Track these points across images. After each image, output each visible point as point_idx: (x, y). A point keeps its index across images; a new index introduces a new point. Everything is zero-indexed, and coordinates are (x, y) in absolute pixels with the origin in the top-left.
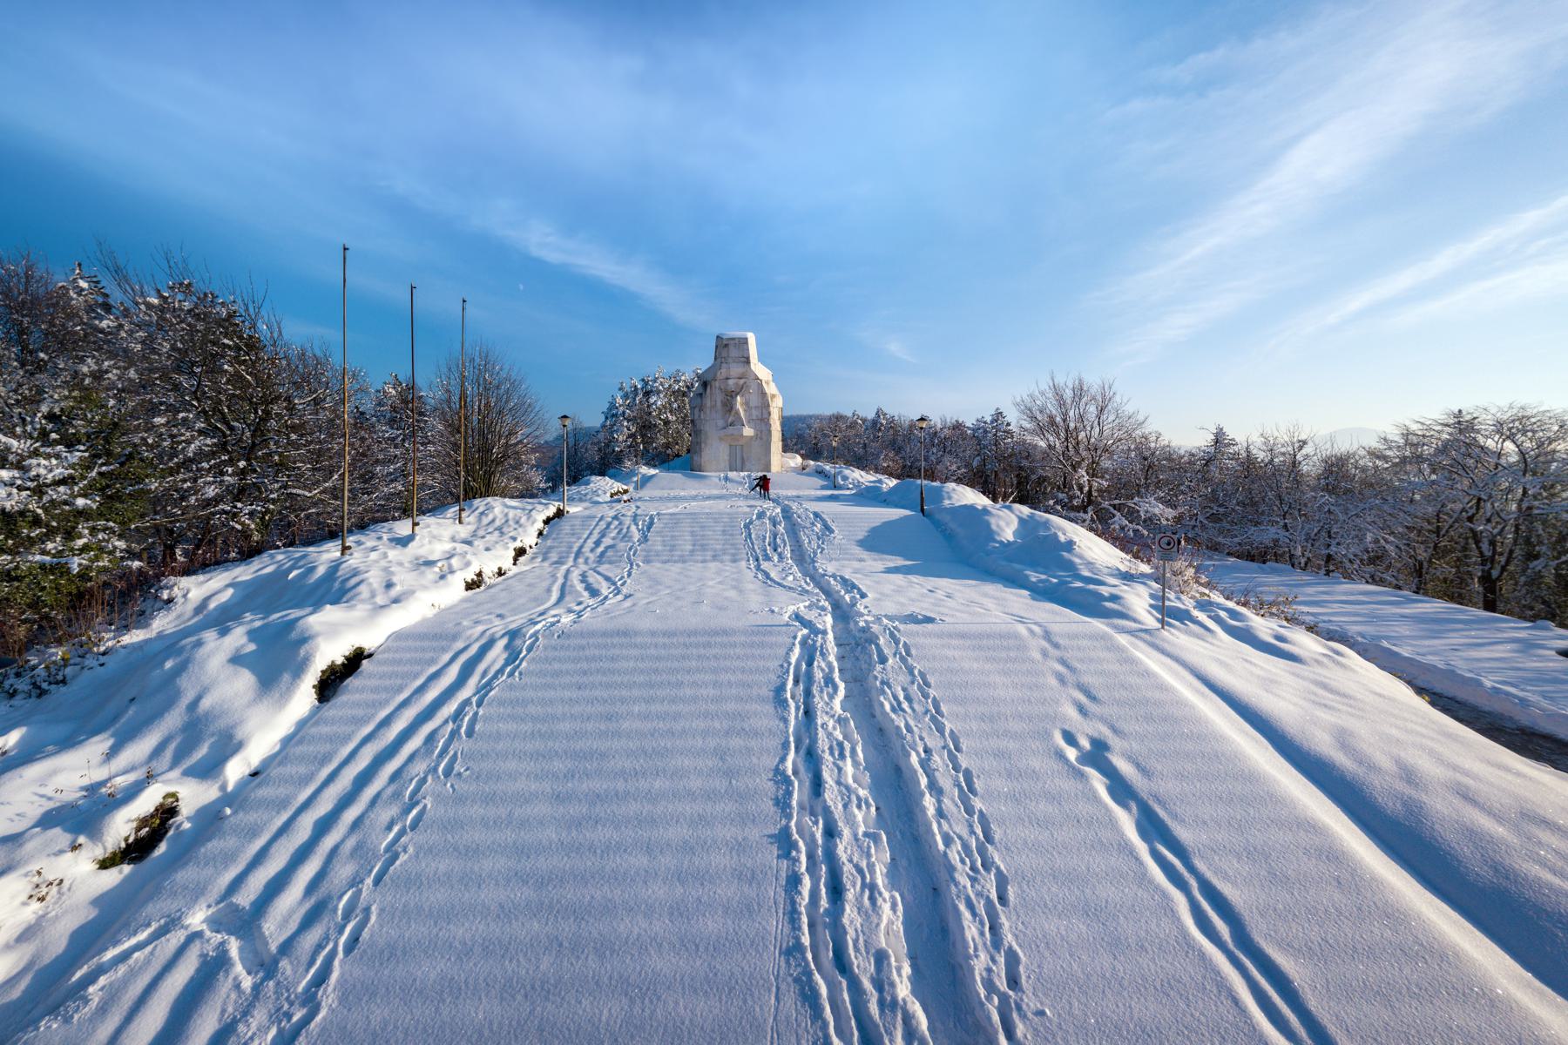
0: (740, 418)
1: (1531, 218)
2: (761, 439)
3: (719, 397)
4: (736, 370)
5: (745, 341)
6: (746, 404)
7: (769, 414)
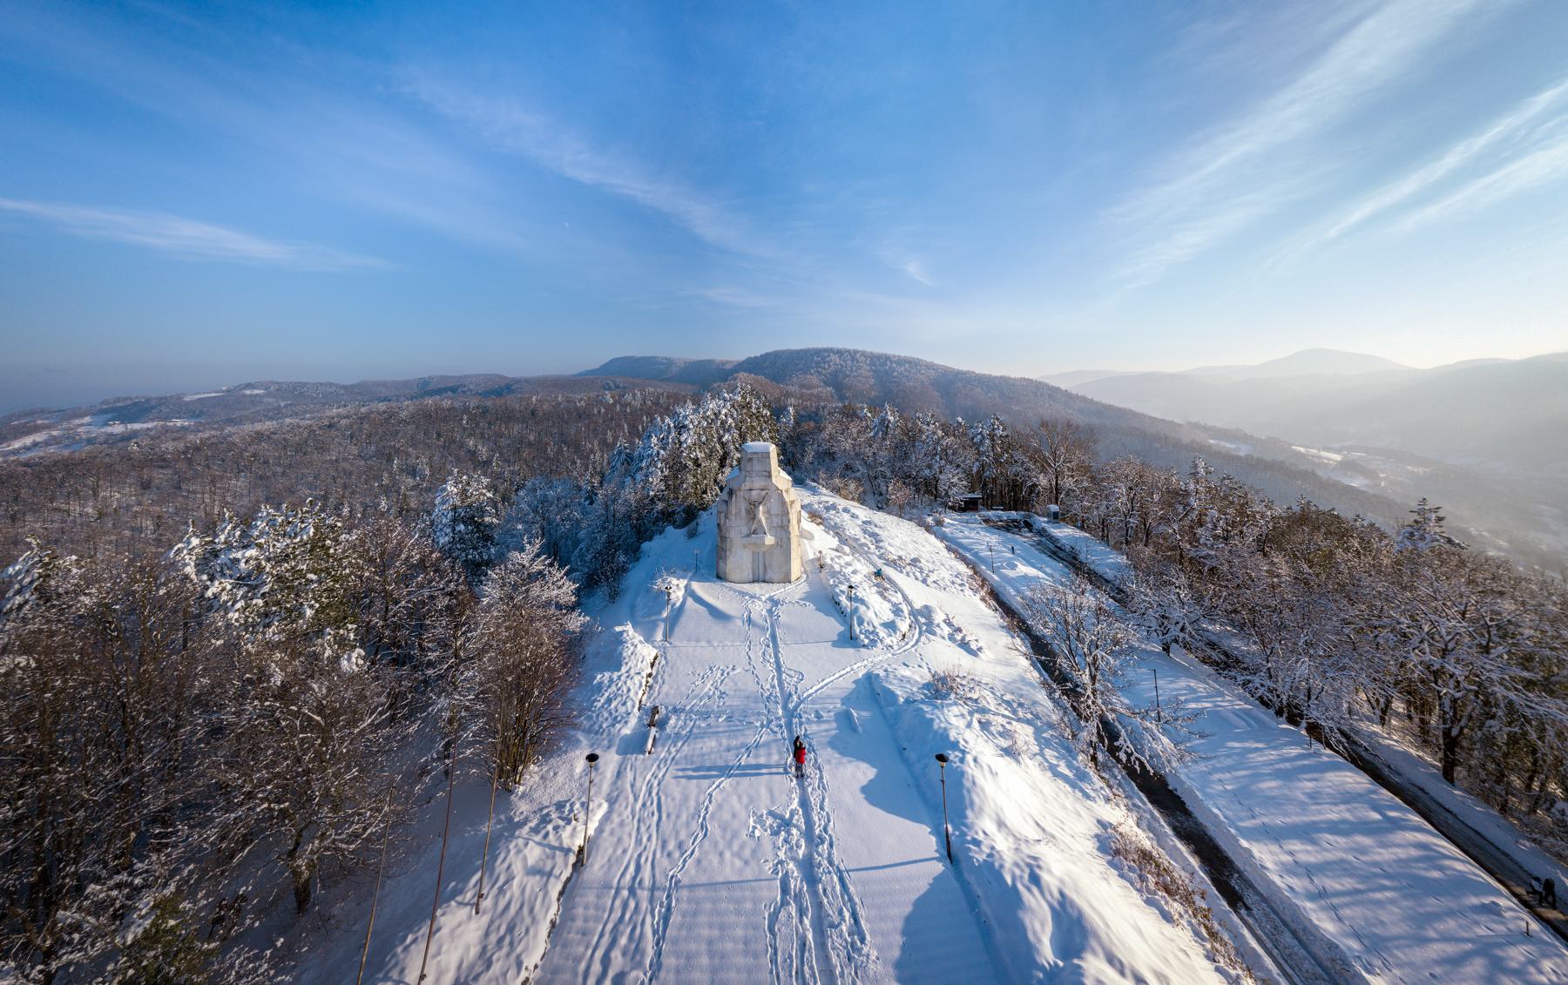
0: (762, 526)
1: (1545, 98)
2: (781, 547)
3: (743, 506)
4: (758, 483)
5: (767, 455)
6: (768, 512)
7: (789, 521)
